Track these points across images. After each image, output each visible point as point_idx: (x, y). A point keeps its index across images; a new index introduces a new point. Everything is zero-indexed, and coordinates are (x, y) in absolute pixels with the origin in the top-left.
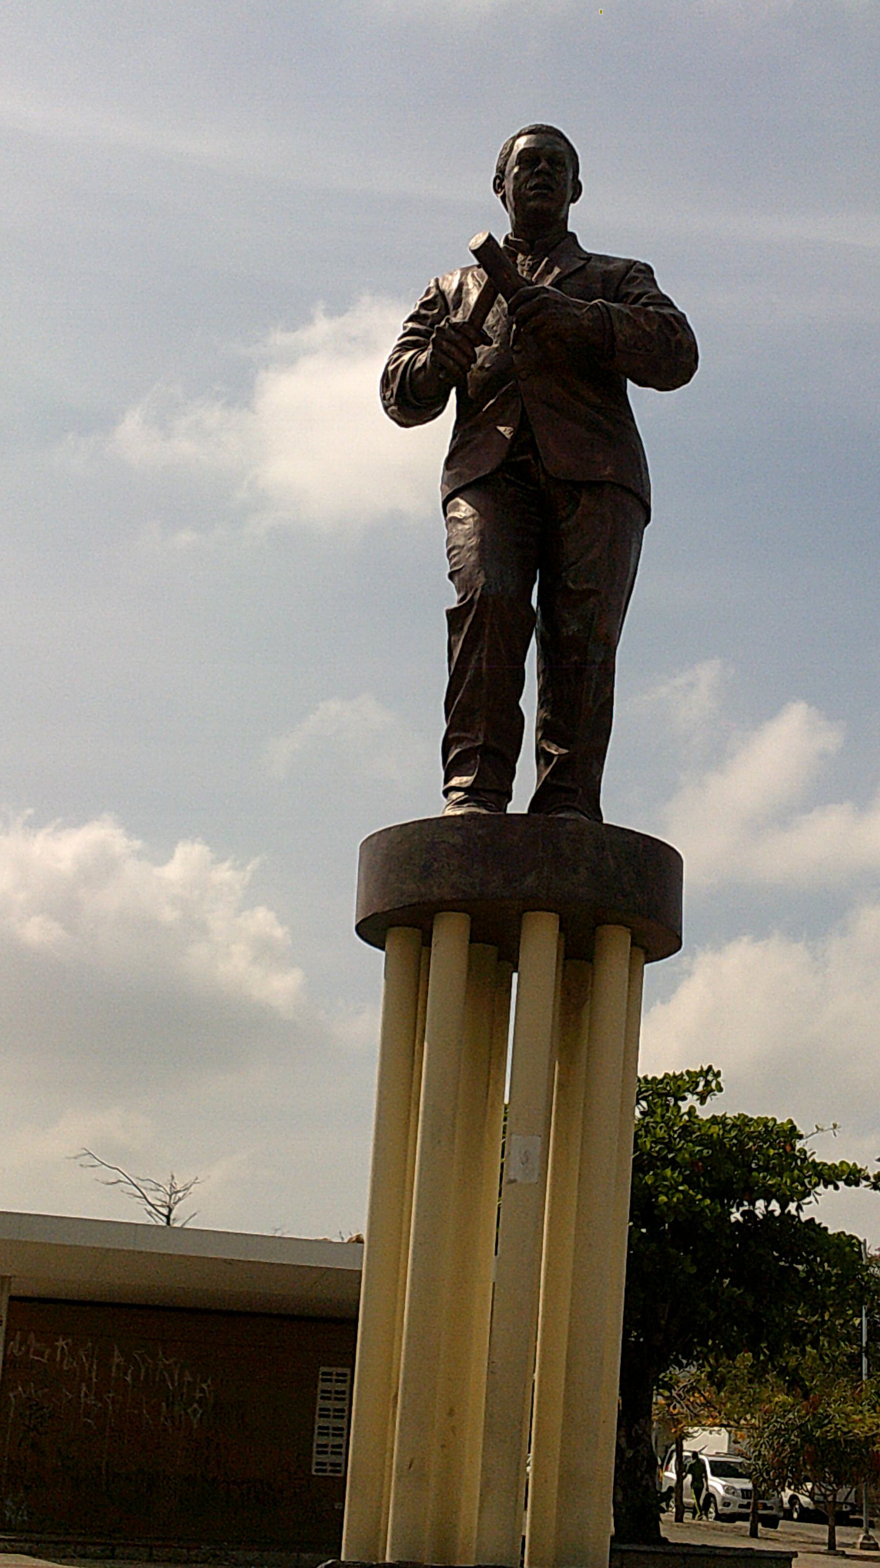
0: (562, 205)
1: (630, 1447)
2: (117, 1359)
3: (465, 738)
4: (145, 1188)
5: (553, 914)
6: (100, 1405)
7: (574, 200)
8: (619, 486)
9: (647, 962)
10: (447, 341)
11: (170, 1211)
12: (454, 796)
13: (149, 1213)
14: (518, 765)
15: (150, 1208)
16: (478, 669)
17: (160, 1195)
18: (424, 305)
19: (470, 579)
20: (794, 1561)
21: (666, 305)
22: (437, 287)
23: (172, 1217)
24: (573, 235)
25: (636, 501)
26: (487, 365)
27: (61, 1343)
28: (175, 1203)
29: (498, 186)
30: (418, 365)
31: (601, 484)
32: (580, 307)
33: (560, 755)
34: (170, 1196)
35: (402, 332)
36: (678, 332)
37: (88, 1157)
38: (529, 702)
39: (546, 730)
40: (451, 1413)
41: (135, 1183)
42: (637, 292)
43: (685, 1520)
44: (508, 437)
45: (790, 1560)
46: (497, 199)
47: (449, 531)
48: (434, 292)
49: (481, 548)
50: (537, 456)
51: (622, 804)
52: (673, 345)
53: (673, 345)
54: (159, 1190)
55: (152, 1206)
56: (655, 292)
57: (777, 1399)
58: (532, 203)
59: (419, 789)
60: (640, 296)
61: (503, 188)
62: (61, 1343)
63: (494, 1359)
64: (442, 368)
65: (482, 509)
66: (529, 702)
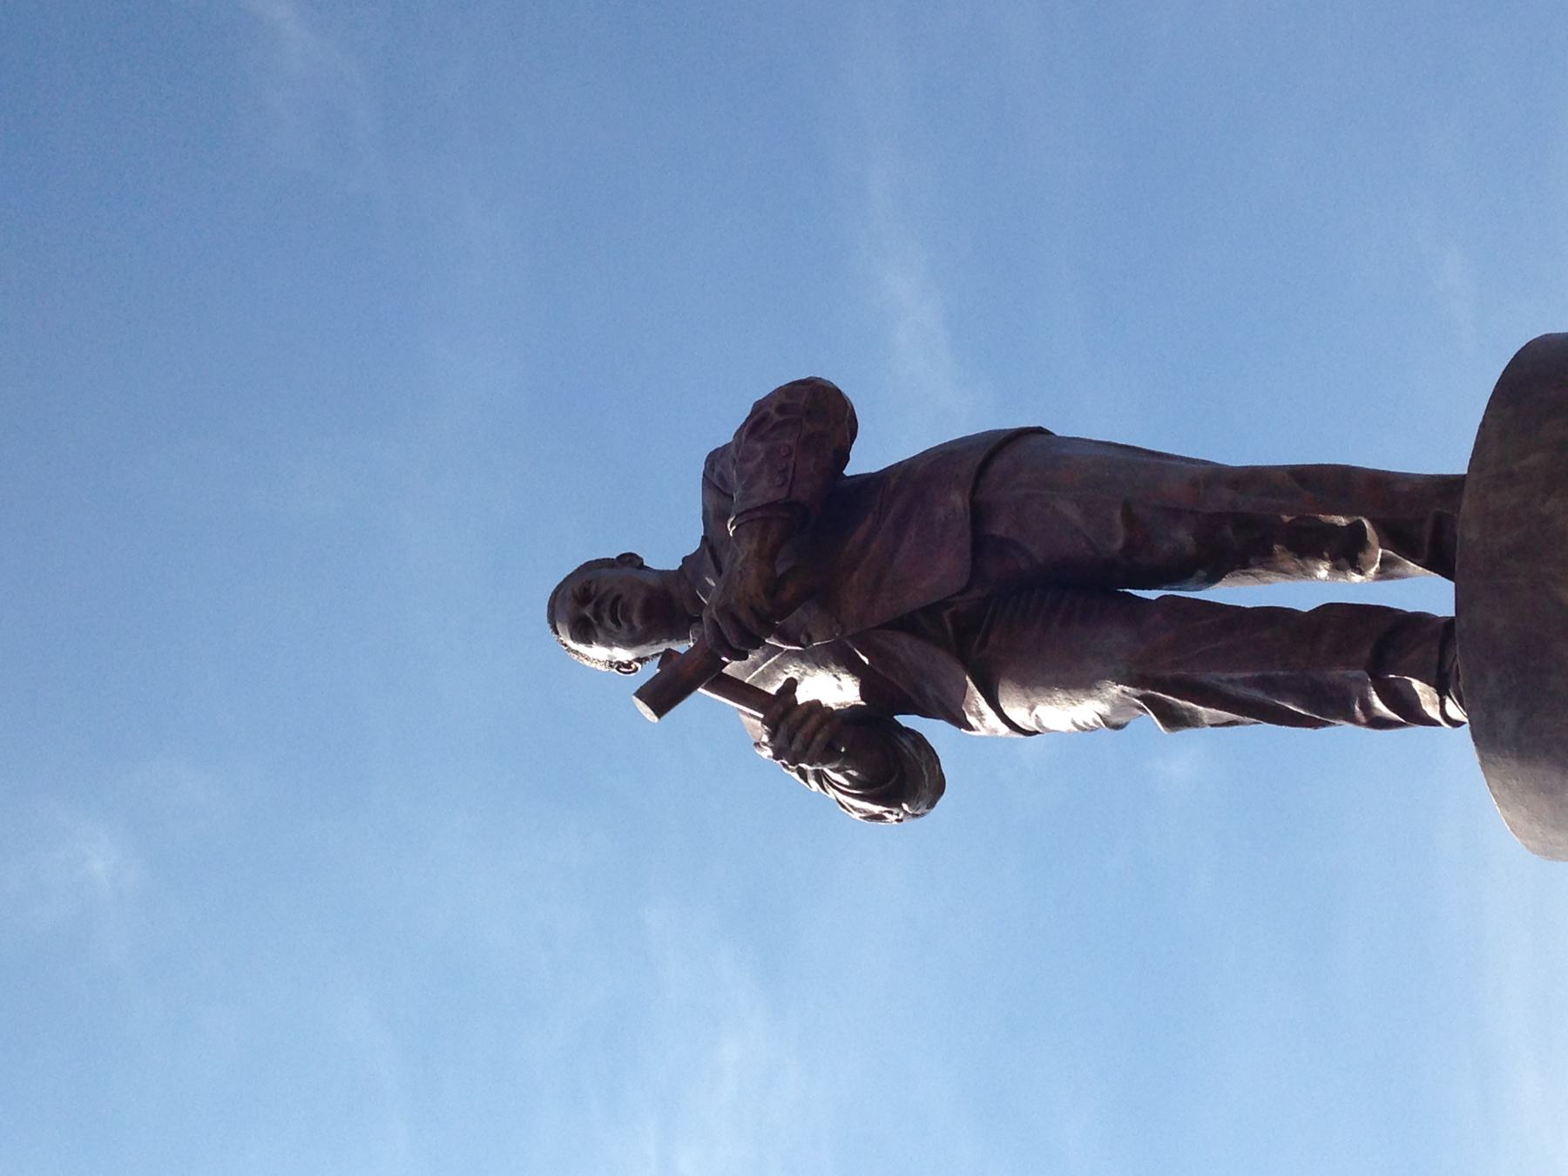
7: (641, 566)
10: (790, 743)
16: (1248, 683)
47: (1203, 725)
50: (944, 604)
51: (1432, 432)
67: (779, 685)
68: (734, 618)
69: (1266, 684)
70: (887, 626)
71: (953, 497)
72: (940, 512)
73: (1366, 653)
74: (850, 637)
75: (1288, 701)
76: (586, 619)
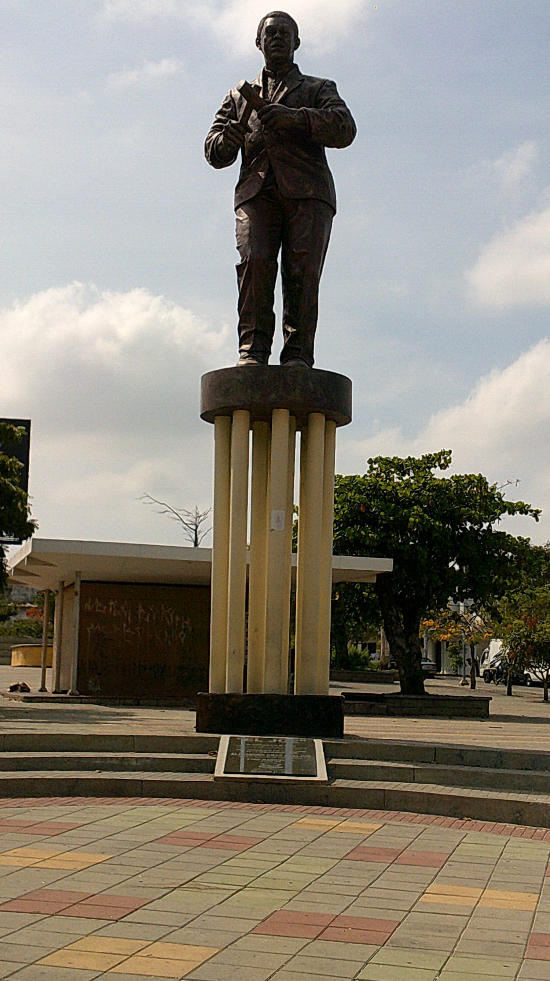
0: (289, 53)
1: (407, 647)
2: (141, 610)
3: (248, 327)
4: (182, 515)
5: (286, 410)
6: (133, 633)
7: (295, 49)
8: (316, 199)
9: (338, 426)
10: (230, 133)
11: (197, 527)
12: (243, 354)
13: (185, 528)
14: (274, 338)
15: (185, 526)
17: (190, 518)
18: (225, 106)
19: (244, 252)
20: (491, 702)
21: (340, 105)
22: (231, 95)
23: (198, 530)
24: (296, 66)
25: (326, 205)
26: (253, 140)
27: (112, 603)
28: (199, 523)
29: (258, 43)
30: (219, 142)
31: (307, 199)
32: (292, 112)
33: (292, 332)
34: (196, 519)
35: (215, 119)
36: (342, 121)
37: (147, 498)
38: (278, 308)
39: (287, 321)
40: (256, 630)
41: (175, 511)
42: (327, 98)
43: (476, 688)
44: (263, 177)
45: (488, 701)
46: (257, 49)
48: (229, 98)
49: (249, 235)
50: (277, 186)
51: (324, 359)
52: (340, 128)
53: (340, 128)
54: (189, 516)
55: (186, 524)
56: (334, 97)
57: (515, 622)
58: (273, 54)
59: (226, 352)
60: (327, 100)
61: (260, 44)
62: (112, 603)
63: (269, 607)
64: (229, 145)
65: (250, 214)
66: (278, 308)
67: (251, 126)
68: (272, 117)
69: (251, 297)
70: (270, 165)
71: (451, 564)
72: (307, 186)
73: (259, 329)
74: (266, 151)
75: (233, 470)
76: (275, 33)
